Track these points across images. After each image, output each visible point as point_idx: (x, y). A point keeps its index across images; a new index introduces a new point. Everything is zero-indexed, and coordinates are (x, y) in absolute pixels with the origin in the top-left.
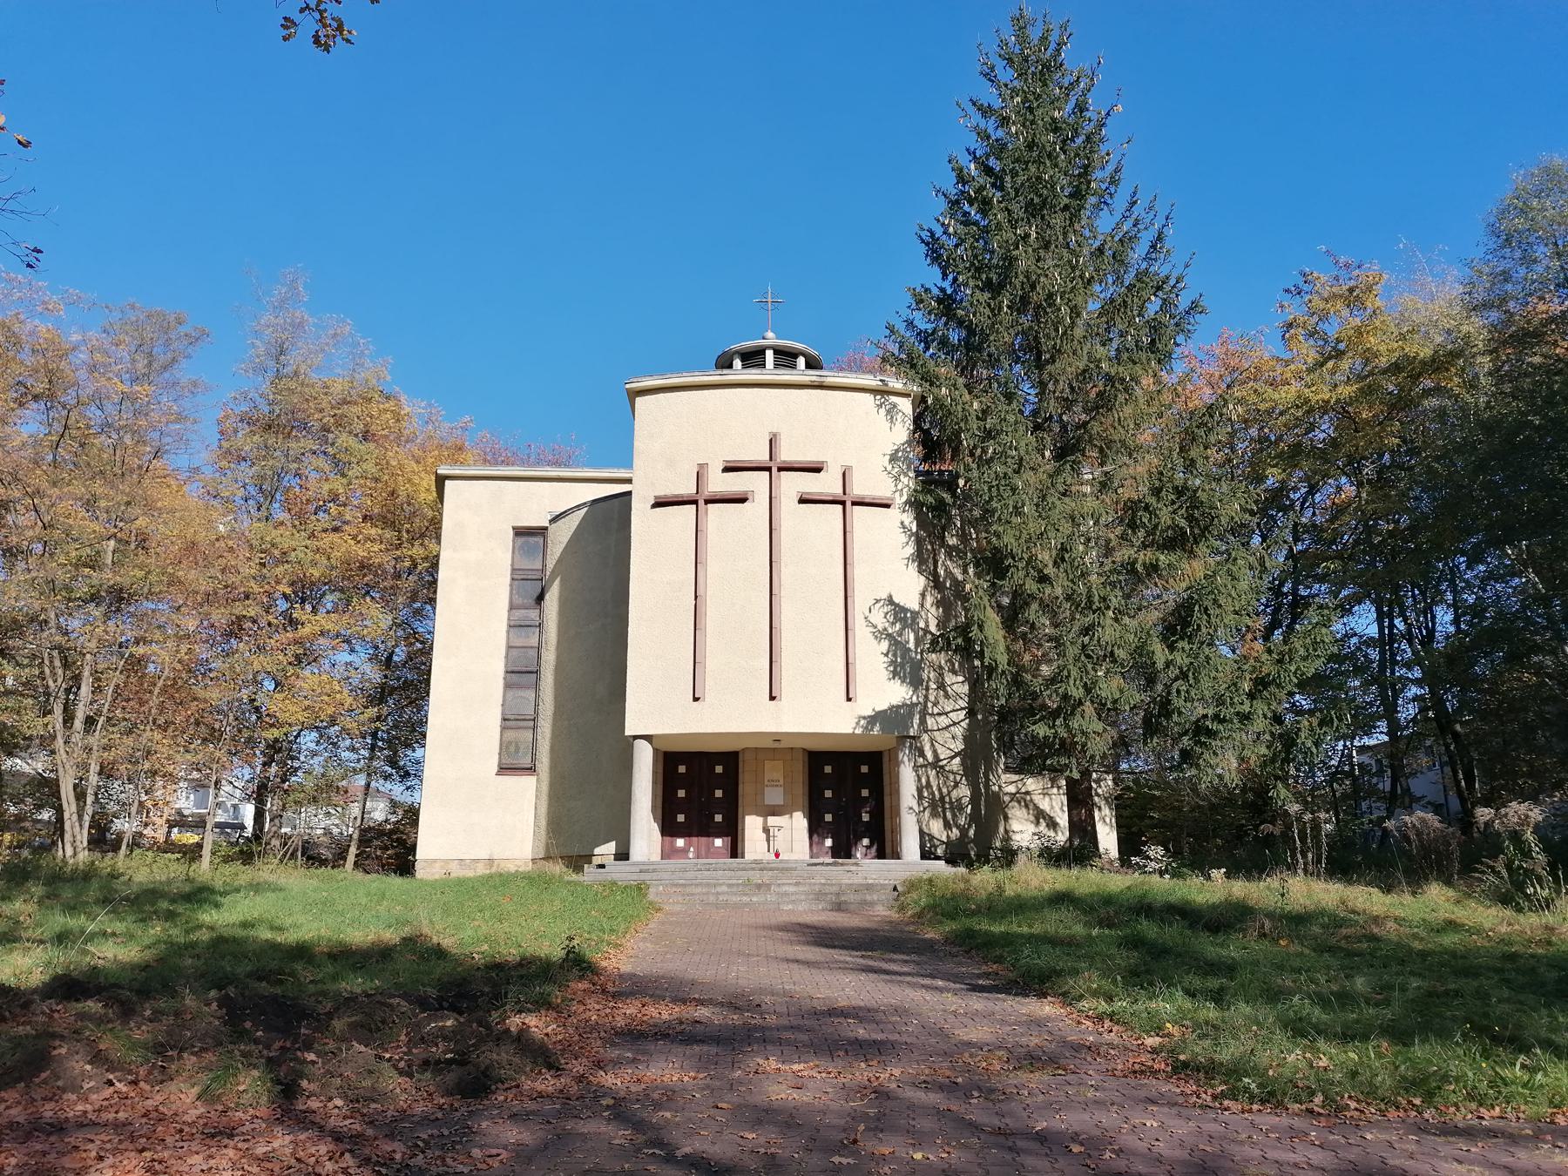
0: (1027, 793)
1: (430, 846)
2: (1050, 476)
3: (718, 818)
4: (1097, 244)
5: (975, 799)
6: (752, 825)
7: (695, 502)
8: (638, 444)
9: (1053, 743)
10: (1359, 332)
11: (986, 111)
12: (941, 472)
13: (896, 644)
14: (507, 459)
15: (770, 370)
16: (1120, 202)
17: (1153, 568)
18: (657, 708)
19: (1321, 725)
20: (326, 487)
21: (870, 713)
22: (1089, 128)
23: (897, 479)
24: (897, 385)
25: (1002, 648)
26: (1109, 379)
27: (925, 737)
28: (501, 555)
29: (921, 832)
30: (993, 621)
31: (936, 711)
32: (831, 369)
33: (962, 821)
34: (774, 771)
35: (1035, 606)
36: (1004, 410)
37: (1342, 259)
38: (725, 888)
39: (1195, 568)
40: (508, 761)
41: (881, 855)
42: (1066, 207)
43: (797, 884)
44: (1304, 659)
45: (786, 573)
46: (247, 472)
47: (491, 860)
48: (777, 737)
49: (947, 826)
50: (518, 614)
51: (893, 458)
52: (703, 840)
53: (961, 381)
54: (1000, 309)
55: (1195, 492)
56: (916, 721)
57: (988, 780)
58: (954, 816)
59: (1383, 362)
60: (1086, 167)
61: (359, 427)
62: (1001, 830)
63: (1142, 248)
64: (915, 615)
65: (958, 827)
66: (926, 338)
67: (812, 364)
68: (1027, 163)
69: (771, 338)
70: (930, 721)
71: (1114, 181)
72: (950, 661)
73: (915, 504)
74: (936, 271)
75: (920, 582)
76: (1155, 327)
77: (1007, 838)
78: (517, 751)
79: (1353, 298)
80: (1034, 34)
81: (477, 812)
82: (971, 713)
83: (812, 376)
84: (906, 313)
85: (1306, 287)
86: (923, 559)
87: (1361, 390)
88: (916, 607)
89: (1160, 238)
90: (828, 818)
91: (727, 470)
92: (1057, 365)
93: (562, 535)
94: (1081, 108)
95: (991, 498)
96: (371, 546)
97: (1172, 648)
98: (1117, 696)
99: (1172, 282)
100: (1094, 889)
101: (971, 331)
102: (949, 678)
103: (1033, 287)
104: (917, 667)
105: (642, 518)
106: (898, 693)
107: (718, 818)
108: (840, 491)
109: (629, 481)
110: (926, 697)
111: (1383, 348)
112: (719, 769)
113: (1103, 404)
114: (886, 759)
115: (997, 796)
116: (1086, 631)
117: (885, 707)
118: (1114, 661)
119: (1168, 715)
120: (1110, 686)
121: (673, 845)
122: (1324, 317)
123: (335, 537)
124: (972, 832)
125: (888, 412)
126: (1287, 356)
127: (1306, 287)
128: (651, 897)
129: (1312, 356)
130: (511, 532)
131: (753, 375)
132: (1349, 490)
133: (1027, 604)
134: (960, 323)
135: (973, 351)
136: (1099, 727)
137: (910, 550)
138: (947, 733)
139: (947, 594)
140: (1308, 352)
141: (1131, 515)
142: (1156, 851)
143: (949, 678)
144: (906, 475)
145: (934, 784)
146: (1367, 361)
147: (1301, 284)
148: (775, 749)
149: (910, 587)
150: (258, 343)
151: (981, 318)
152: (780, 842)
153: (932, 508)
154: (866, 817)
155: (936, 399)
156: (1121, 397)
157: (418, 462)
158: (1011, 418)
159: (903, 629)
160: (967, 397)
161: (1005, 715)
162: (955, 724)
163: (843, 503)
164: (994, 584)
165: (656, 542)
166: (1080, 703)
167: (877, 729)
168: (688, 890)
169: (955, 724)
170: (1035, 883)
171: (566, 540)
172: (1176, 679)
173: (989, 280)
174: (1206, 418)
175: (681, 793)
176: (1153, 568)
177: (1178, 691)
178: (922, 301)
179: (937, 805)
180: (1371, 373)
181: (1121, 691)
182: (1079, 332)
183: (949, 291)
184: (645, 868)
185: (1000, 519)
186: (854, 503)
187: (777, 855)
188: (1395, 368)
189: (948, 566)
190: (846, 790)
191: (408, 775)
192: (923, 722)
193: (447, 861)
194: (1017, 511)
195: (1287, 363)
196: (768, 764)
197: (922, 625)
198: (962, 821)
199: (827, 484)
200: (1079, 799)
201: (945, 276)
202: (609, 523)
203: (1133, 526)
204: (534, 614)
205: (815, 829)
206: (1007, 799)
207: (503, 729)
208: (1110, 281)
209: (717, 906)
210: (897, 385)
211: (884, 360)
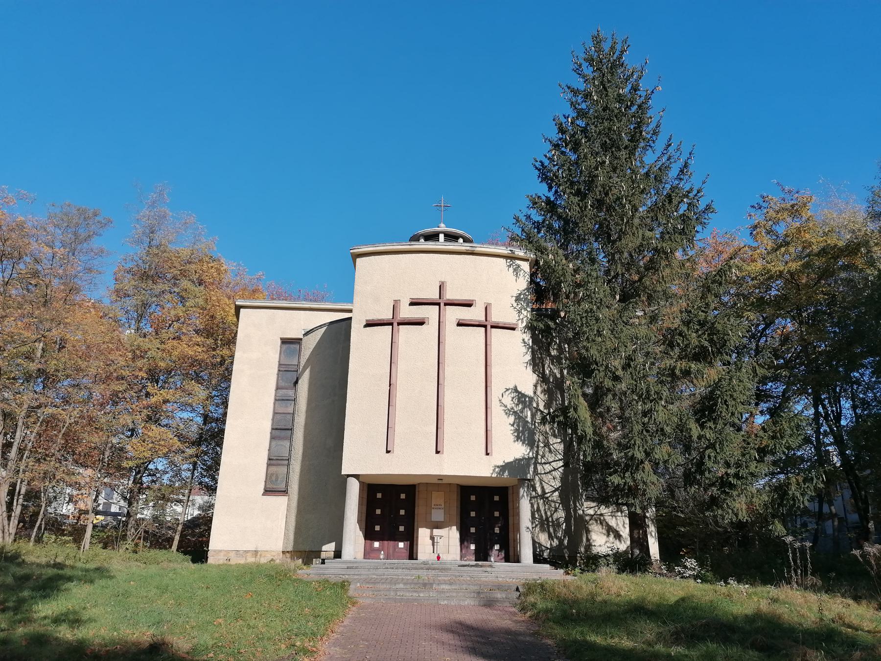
0: (602, 515)
1: (220, 541)
2: (619, 312)
3: (402, 528)
4: (645, 170)
5: (567, 519)
6: (423, 534)
7: (391, 324)
8: (358, 287)
9: (623, 490)
10: (799, 230)
11: (575, 92)
12: (546, 309)
13: (519, 418)
14: (283, 298)
15: (442, 243)
16: (660, 144)
17: (687, 373)
18: (363, 456)
19: (805, 481)
20: (173, 312)
21: (501, 463)
22: (639, 101)
23: (520, 312)
24: (520, 253)
25: (589, 423)
26: (656, 250)
27: (537, 478)
28: (272, 355)
29: (534, 542)
30: (583, 404)
31: (543, 461)
32: (478, 243)
33: (560, 534)
34: (438, 499)
35: (610, 396)
36: (587, 268)
37: (787, 188)
38: (401, 586)
39: (714, 372)
40: (270, 486)
41: (507, 559)
42: (626, 147)
43: (451, 584)
44: (791, 436)
45: (448, 370)
46: (130, 303)
47: (256, 552)
48: (440, 478)
49: (550, 537)
50: (281, 392)
51: (518, 299)
52: (392, 542)
53: (561, 252)
54: (586, 207)
55: (713, 324)
56: (532, 469)
57: (575, 506)
58: (555, 531)
59: (815, 248)
60: (638, 123)
61: (195, 277)
62: (584, 539)
63: (674, 172)
64: (531, 399)
65: (557, 538)
66: (538, 226)
67: (466, 240)
68: (603, 119)
69: (443, 227)
70: (539, 467)
71: (655, 133)
72: (552, 428)
73: (531, 328)
74: (545, 186)
75: (532, 378)
76: (684, 219)
77: (589, 546)
78: (277, 480)
79: (794, 211)
80: (606, 47)
81: (250, 521)
82: (566, 465)
83: (466, 247)
84: (525, 211)
85: (765, 205)
86: (536, 364)
87: (803, 265)
88: (531, 394)
89: (686, 165)
90: (473, 530)
91: (412, 304)
92: (623, 241)
93: (310, 344)
94: (635, 89)
95: (582, 325)
96: (192, 348)
97: (702, 426)
98: (666, 458)
99: (695, 192)
100: (656, 599)
101: (567, 221)
102: (552, 440)
103: (607, 194)
104: (532, 433)
105: (357, 332)
106: (520, 451)
107: (402, 528)
108: (483, 319)
109: (350, 311)
110: (537, 452)
111: (813, 240)
112: (403, 496)
113: (651, 266)
114: (510, 492)
115: (581, 517)
116: (645, 414)
117: (511, 460)
118: (664, 434)
119: (702, 473)
120: (661, 452)
121: (372, 545)
122: (776, 223)
123: (175, 342)
124: (566, 542)
125: (515, 270)
126: (755, 245)
127: (765, 205)
128: (351, 593)
129: (770, 246)
130: (279, 342)
131: (431, 245)
132: (790, 327)
133: (606, 394)
134: (560, 217)
135: (567, 232)
136: (654, 478)
137: (528, 357)
138: (550, 476)
139: (552, 387)
140: (768, 242)
141: (669, 340)
142: (691, 563)
143: (552, 440)
144: (525, 309)
145: (542, 508)
146: (804, 248)
147: (761, 203)
148: (440, 484)
149: (527, 381)
150: (138, 226)
151: (573, 213)
152: (441, 543)
153: (542, 331)
154: (497, 530)
155: (545, 262)
156: (663, 263)
157: (229, 298)
158: (594, 274)
159: (523, 408)
160: (564, 261)
161: (589, 467)
162: (555, 470)
163: (485, 326)
164: (584, 381)
165: (366, 350)
166: (642, 462)
167: (506, 473)
168: (378, 586)
169: (555, 470)
170: (614, 590)
171: (312, 347)
172: (707, 448)
173: (579, 190)
174: (718, 277)
175: (378, 512)
176: (687, 373)
177: (709, 457)
178: (536, 203)
179: (544, 523)
180: (808, 255)
181: (669, 455)
182: (636, 221)
183: (552, 199)
184: (352, 566)
185: (588, 338)
186: (492, 327)
187: (438, 558)
188: (823, 252)
189: (549, 368)
190: (483, 513)
191: (212, 490)
192: (535, 468)
193: (228, 552)
194: (599, 333)
195: (755, 249)
196: (435, 494)
197: (535, 405)
198: (560, 534)
199: (475, 314)
200: (637, 523)
201: (550, 188)
202: (338, 335)
203: (671, 345)
204: (291, 393)
205: (464, 539)
206: (587, 518)
207: (268, 465)
208: (653, 193)
209: (395, 600)
210: (520, 253)
211: (512, 239)
